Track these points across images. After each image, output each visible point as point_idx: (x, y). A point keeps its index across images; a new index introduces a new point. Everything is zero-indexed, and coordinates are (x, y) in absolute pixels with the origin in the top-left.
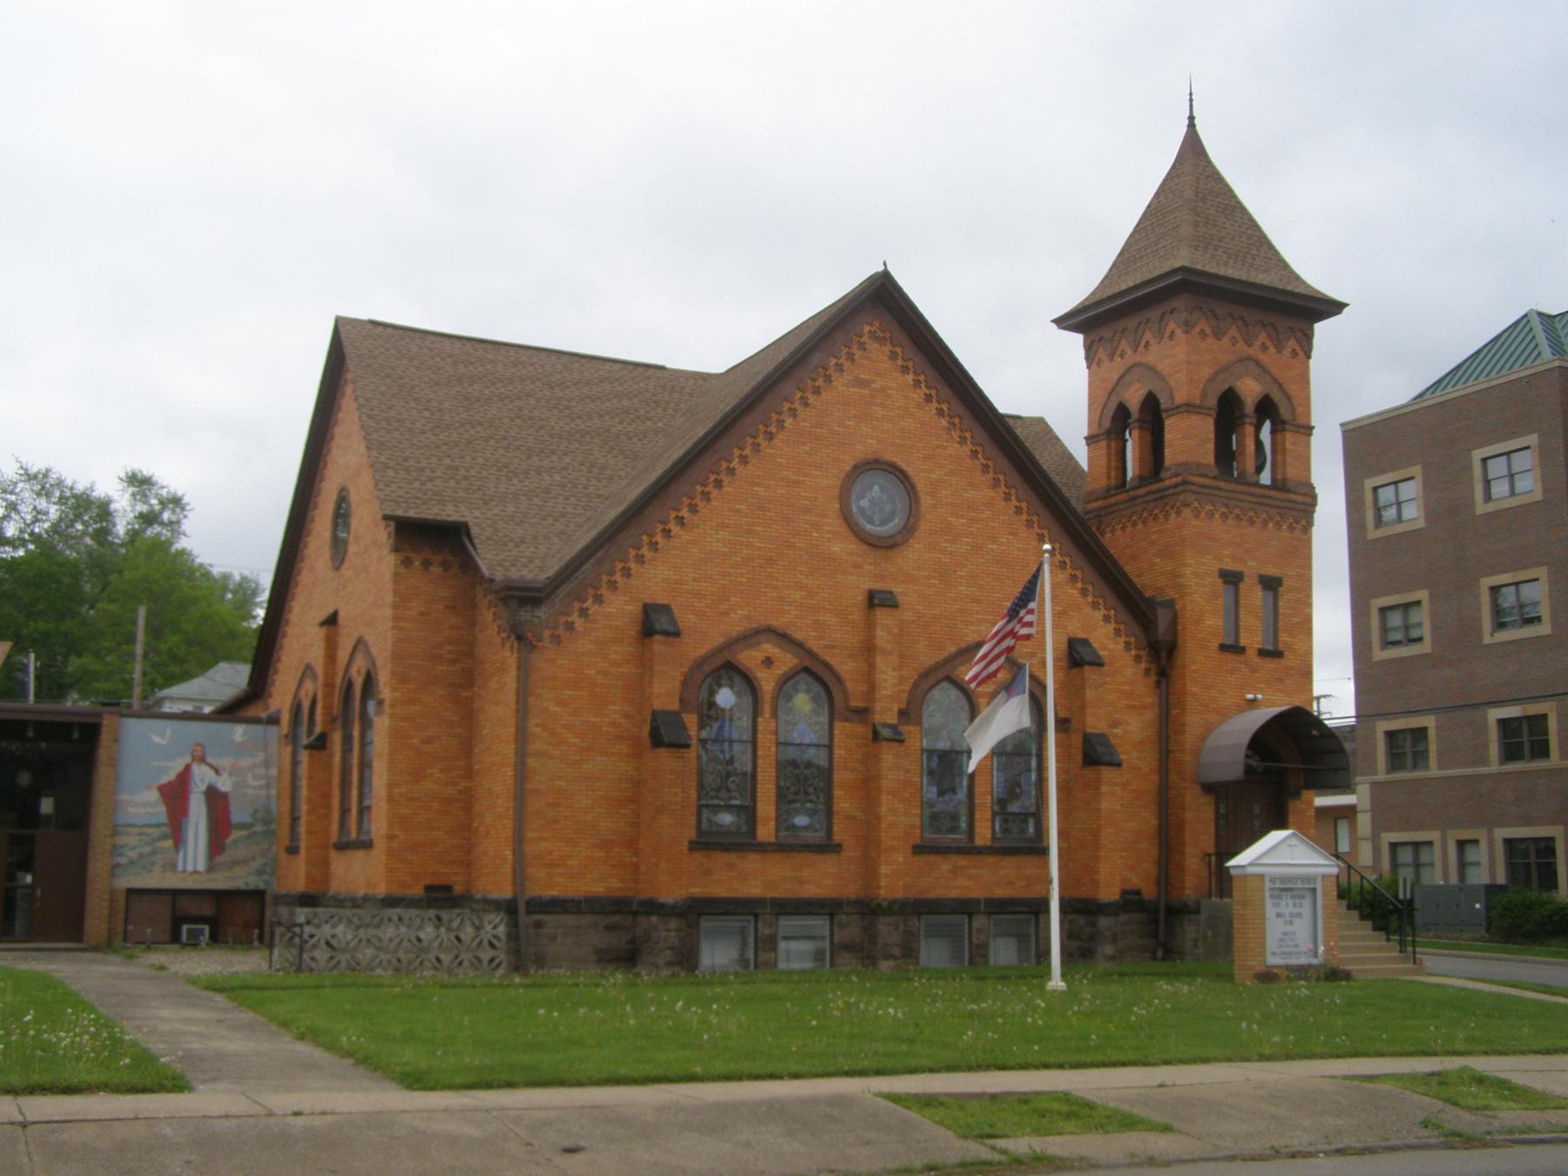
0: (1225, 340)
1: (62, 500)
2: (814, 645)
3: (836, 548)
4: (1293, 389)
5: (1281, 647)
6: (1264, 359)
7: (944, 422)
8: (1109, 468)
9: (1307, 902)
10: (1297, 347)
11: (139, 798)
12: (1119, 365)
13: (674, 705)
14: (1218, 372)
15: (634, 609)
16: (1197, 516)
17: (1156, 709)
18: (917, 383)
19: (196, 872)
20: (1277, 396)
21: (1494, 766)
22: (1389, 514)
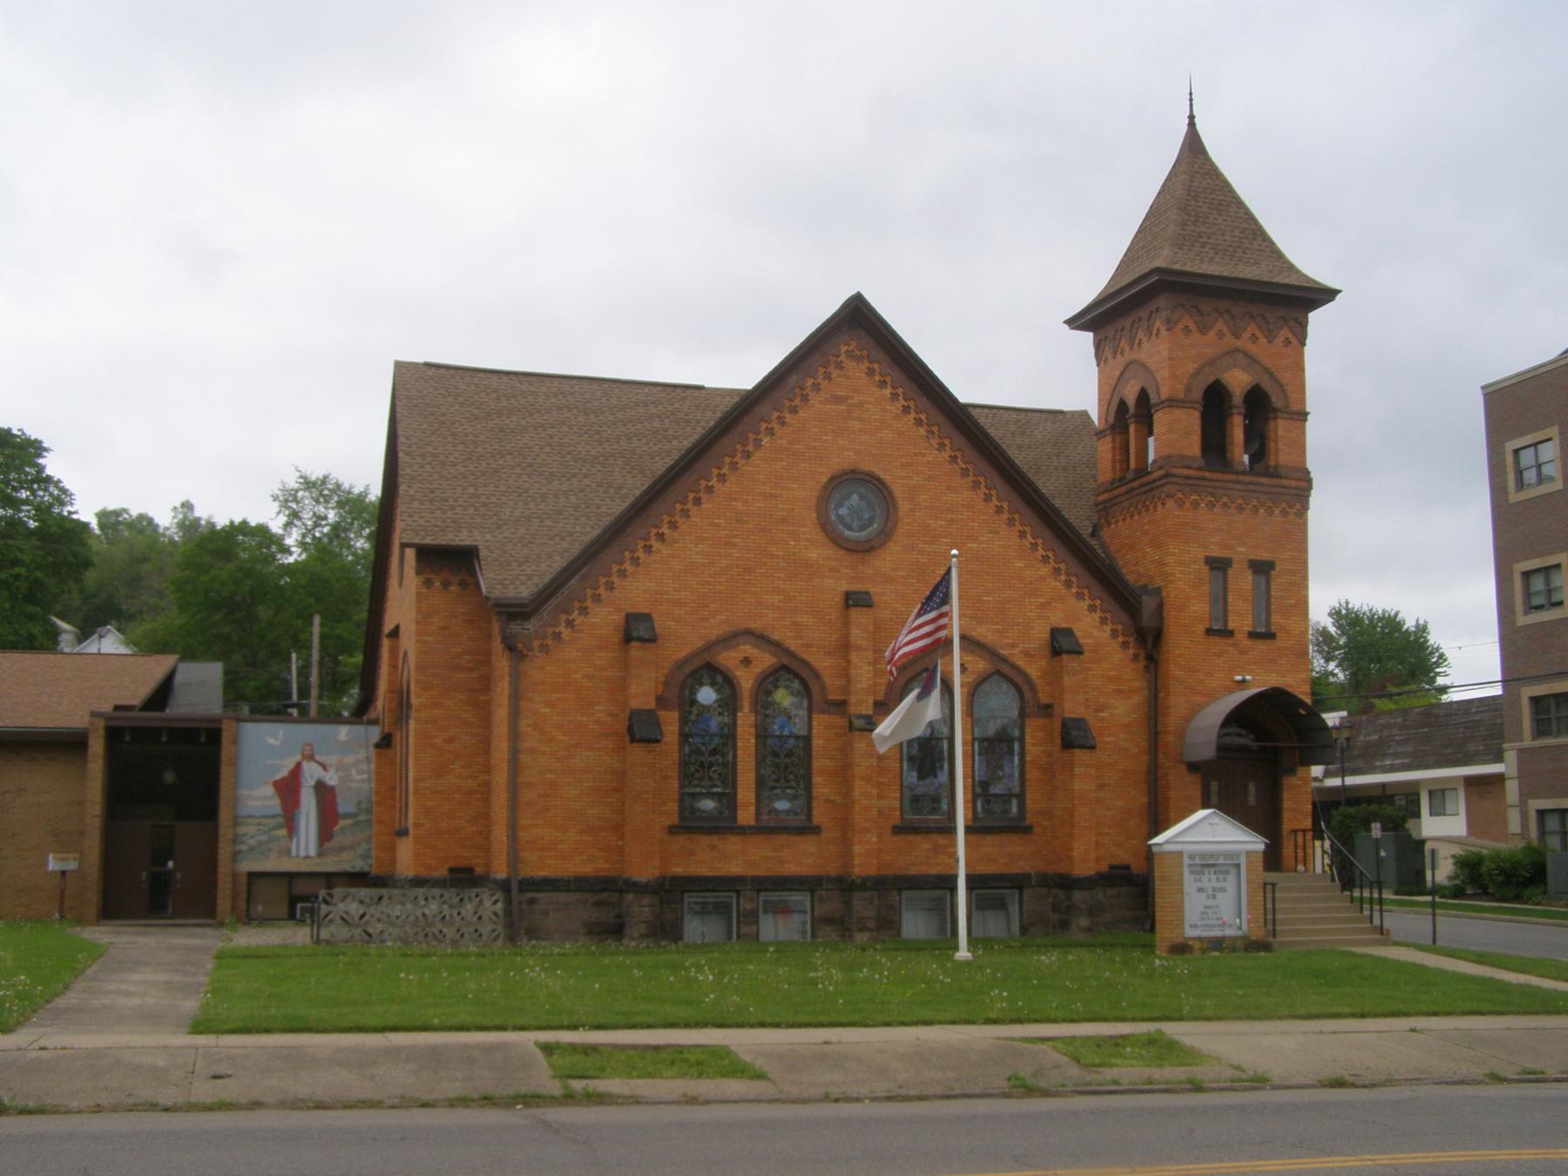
0: (1212, 334)
1: (340, 505)
2: (792, 644)
3: (813, 554)
5: (1273, 629)
6: (1250, 347)
7: (922, 431)
8: (1114, 461)
9: (1231, 878)
10: (1290, 336)
11: (255, 793)
12: (1120, 361)
13: (652, 705)
15: (617, 618)
16: (1180, 507)
17: (1146, 692)
18: (895, 396)
19: (308, 857)
20: (1267, 385)
22: (1530, 476)
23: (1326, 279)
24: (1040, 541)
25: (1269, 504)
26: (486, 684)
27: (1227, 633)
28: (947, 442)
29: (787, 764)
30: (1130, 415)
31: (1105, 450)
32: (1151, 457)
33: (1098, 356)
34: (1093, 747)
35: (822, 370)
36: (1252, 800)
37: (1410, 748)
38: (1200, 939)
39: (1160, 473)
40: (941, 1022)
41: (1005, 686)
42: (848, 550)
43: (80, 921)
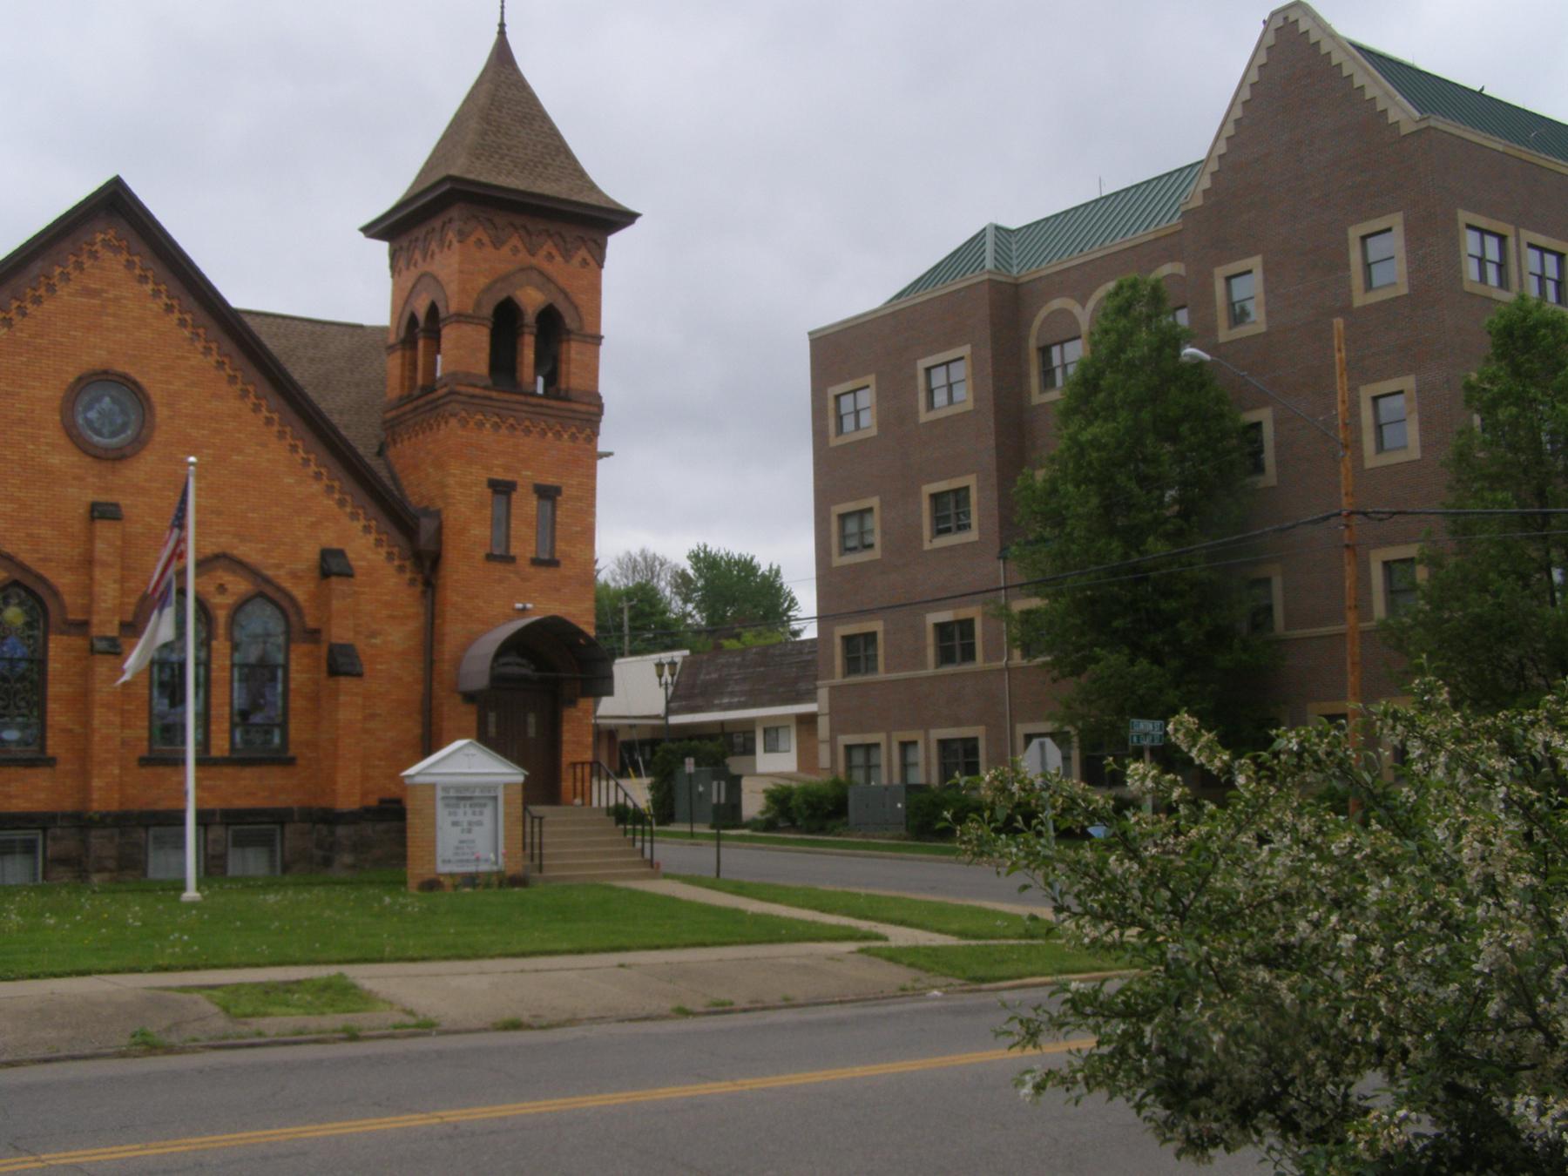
0: (506, 250)
2: (27, 558)
5: (558, 556)
6: (548, 267)
7: (187, 333)
8: (402, 377)
9: (488, 811)
14: (495, 282)
20: (561, 306)
21: (931, 670)
23: (624, 198)
24: (312, 457)
25: (558, 427)
27: (508, 559)
28: (214, 346)
30: (419, 328)
32: (439, 374)
34: (360, 675)
35: (72, 259)
36: (532, 732)
37: (746, 687)
38: (451, 875)
39: (445, 390)
40: (101, 972)
41: (269, 610)
42: (96, 457)
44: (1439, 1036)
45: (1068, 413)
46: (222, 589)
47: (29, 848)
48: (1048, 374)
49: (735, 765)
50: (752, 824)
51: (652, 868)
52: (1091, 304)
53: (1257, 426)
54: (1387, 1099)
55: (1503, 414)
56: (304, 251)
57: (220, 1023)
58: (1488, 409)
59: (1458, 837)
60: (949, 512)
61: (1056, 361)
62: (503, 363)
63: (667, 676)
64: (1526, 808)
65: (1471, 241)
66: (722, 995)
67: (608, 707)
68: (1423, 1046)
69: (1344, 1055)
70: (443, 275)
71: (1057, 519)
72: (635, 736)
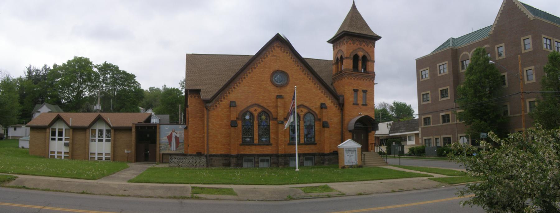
0: (355, 45)
2: (265, 106)
4: (370, 54)
6: (363, 48)
9: (354, 153)
15: (228, 102)
20: (367, 55)
21: (441, 124)
26: (203, 116)
27: (357, 104)
29: (266, 131)
30: (339, 60)
31: (334, 67)
33: (334, 49)
41: (311, 115)
43: (131, 162)
44: (541, 191)
45: (467, 74)
46: (302, 111)
47: (268, 161)
48: (463, 66)
49: (403, 143)
50: (406, 155)
51: (387, 163)
52: (471, 53)
53: (504, 76)
54: (532, 204)
55: (551, 73)
56: (317, 47)
57: (303, 194)
58: (548, 72)
59: (544, 154)
60: (444, 93)
61: (465, 64)
62: (355, 66)
63: (389, 126)
64: (557, 147)
65: (544, 41)
66: (401, 188)
67: (377, 133)
68: (538, 193)
69: (523, 196)
70: (343, 50)
71: (465, 94)
72: (383, 138)
